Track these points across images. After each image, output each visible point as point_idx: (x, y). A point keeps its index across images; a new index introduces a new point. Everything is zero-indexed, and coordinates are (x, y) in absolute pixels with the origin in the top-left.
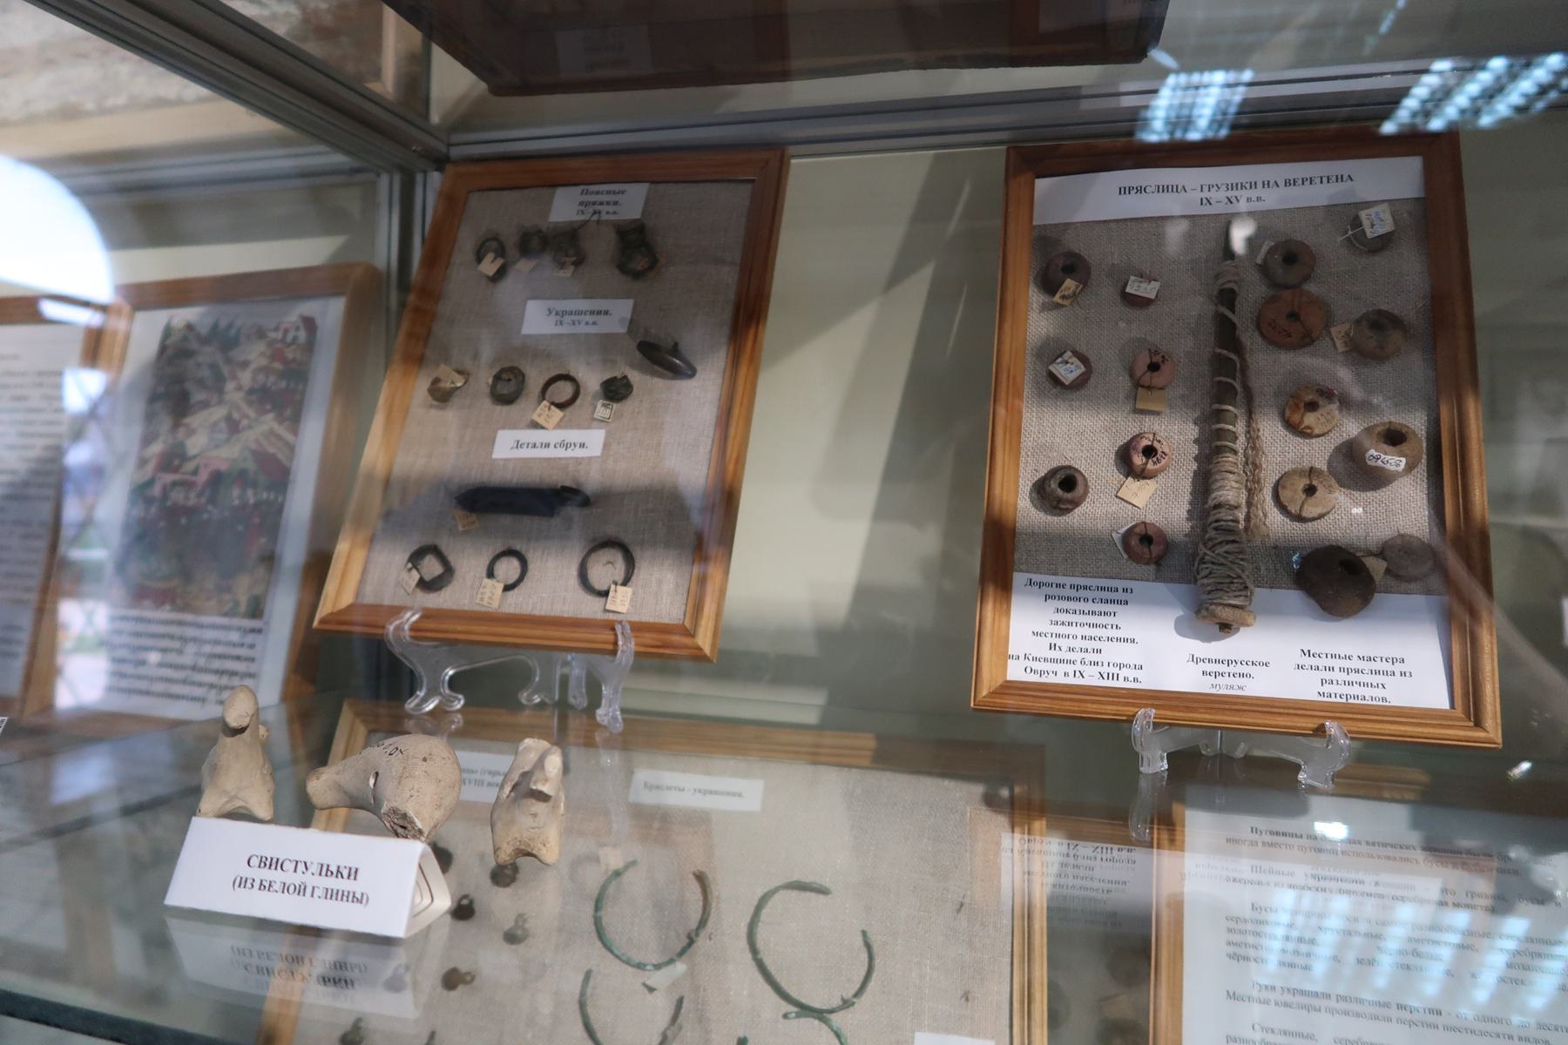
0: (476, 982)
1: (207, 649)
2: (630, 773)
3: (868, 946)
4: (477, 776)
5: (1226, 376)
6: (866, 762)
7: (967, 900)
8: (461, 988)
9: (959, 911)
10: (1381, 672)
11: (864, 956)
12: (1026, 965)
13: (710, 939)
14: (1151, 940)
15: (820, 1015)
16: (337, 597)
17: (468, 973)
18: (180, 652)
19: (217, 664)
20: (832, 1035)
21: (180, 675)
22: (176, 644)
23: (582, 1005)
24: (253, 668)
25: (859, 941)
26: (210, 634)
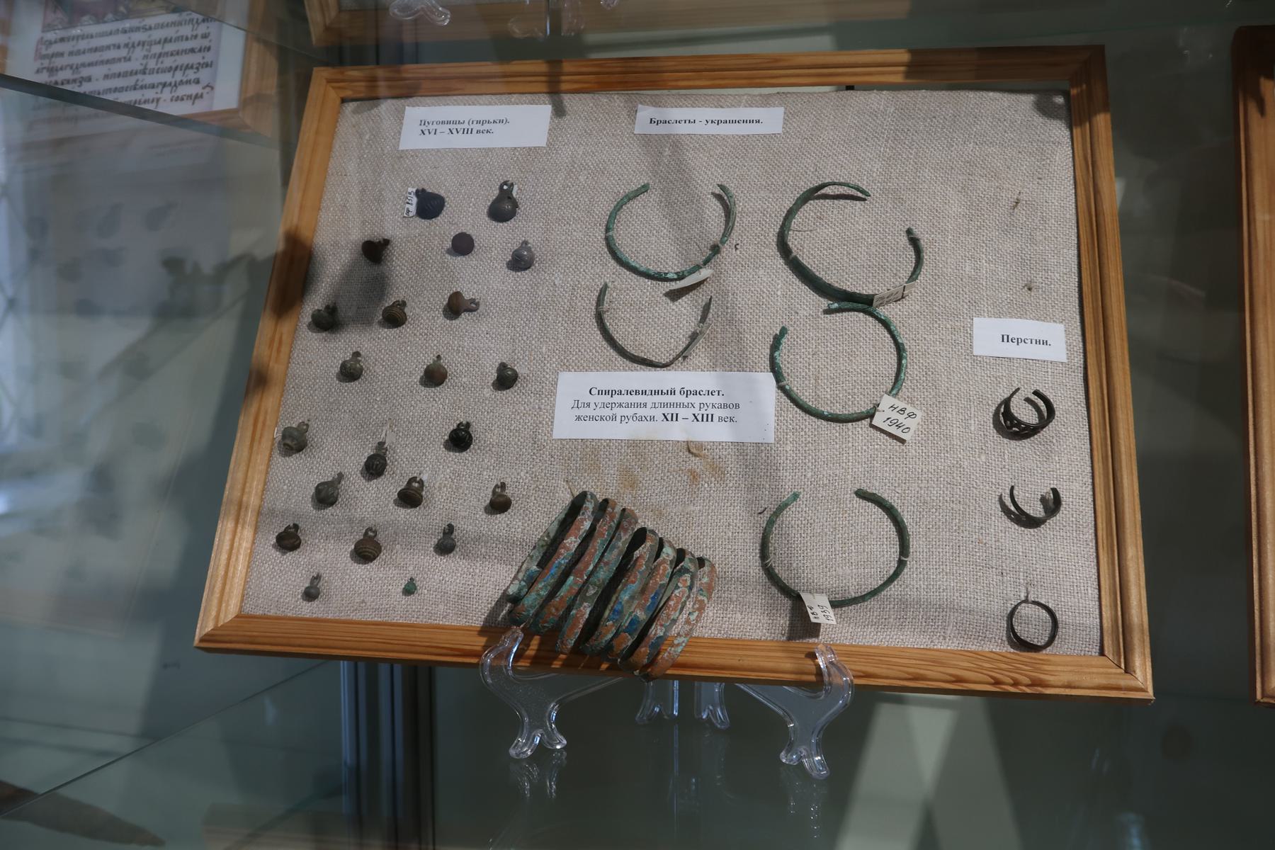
0: (481, 308)
1: (157, 49)
2: (633, 113)
3: (914, 242)
4: (466, 126)
5: (509, 655)
6: (898, 79)
7: (1023, 197)
8: (464, 315)
9: (1014, 207)
10: (1041, 343)
11: (911, 253)
12: (1096, 249)
13: (736, 249)
14: (1129, 304)
15: (863, 303)
16: (225, 616)
17: (473, 301)
18: (128, 59)
19: (168, 62)
20: (879, 326)
21: (130, 81)
22: (123, 53)
23: (600, 318)
24: (209, 57)
25: (904, 240)
26: (158, 34)
